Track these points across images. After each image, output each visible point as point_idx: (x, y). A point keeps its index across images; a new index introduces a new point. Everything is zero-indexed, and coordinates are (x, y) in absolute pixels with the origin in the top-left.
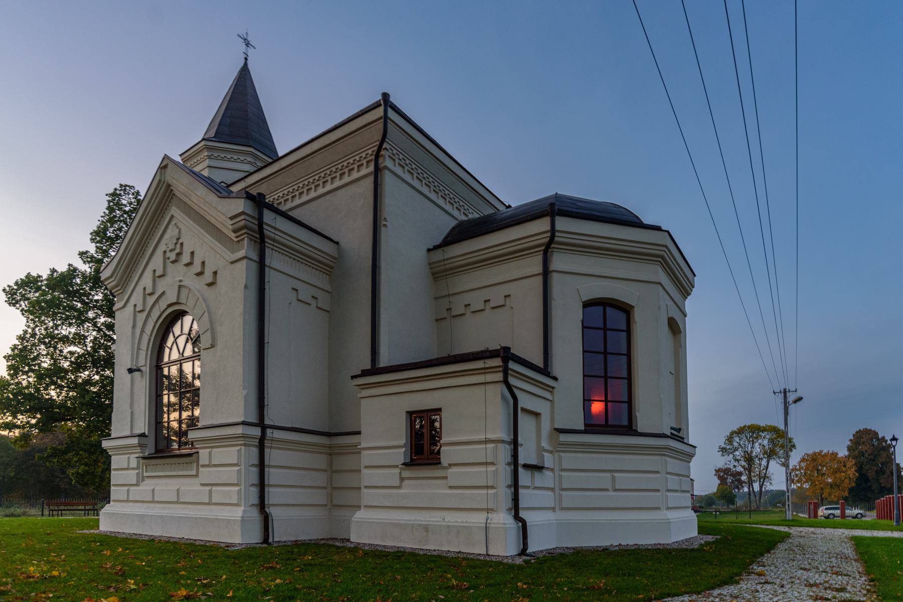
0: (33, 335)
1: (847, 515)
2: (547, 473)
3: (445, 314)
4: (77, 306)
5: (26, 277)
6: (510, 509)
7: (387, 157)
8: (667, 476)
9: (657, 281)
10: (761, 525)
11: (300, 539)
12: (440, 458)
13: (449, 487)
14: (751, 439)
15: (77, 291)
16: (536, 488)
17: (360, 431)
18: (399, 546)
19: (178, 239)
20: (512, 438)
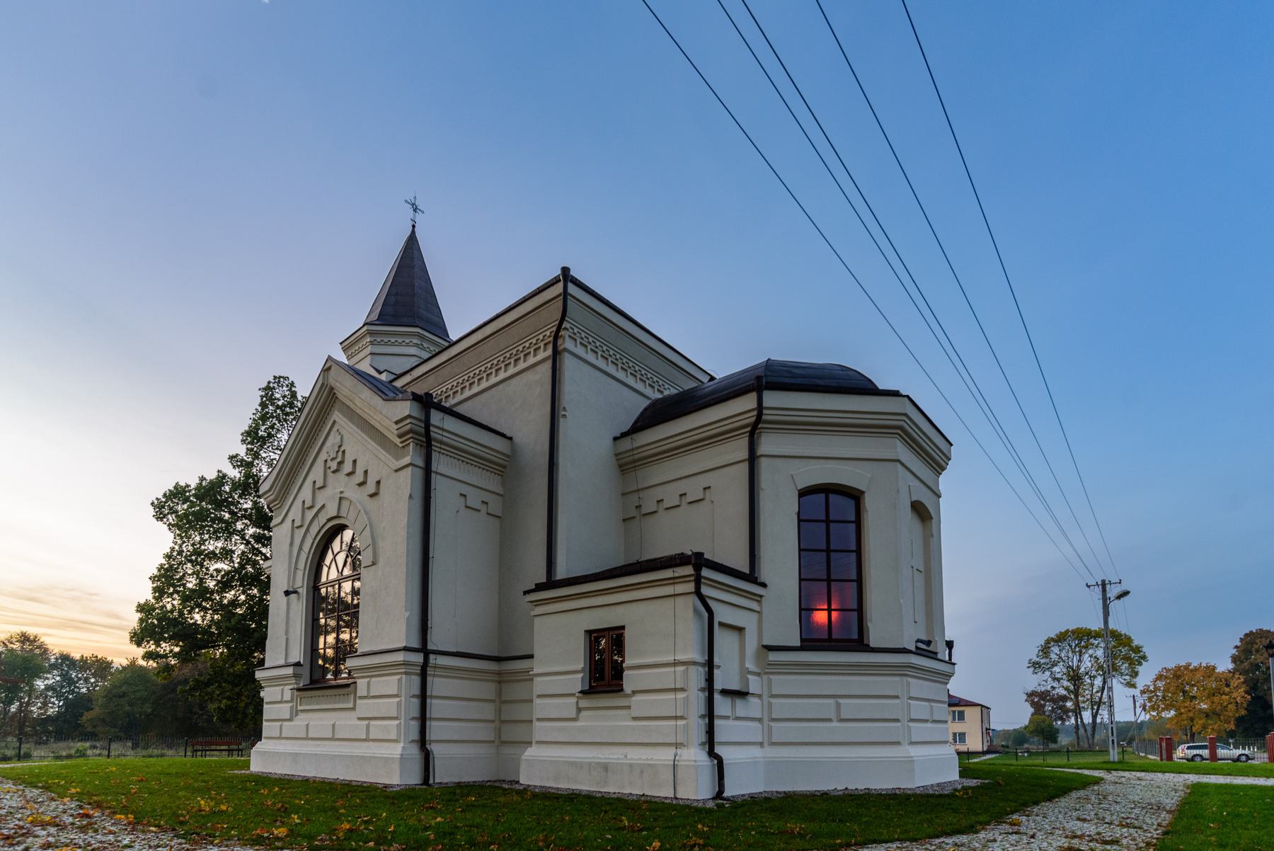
0: (180, 553)
1: (1220, 757)
2: (752, 700)
3: (633, 513)
4: (225, 516)
5: (175, 487)
6: (703, 744)
7: (567, 338)
8: (910, 701)
9: (896, 458)
10: (1069, 768)
11: (463, 781)
12: (622, 684)
13: (633, 718)
14: (1077, 649)
15: (226, 500)
16: (737, 718)
17: (533, 655)
18: (574, 788)
19: (340, 447)
20: (707, 658)
